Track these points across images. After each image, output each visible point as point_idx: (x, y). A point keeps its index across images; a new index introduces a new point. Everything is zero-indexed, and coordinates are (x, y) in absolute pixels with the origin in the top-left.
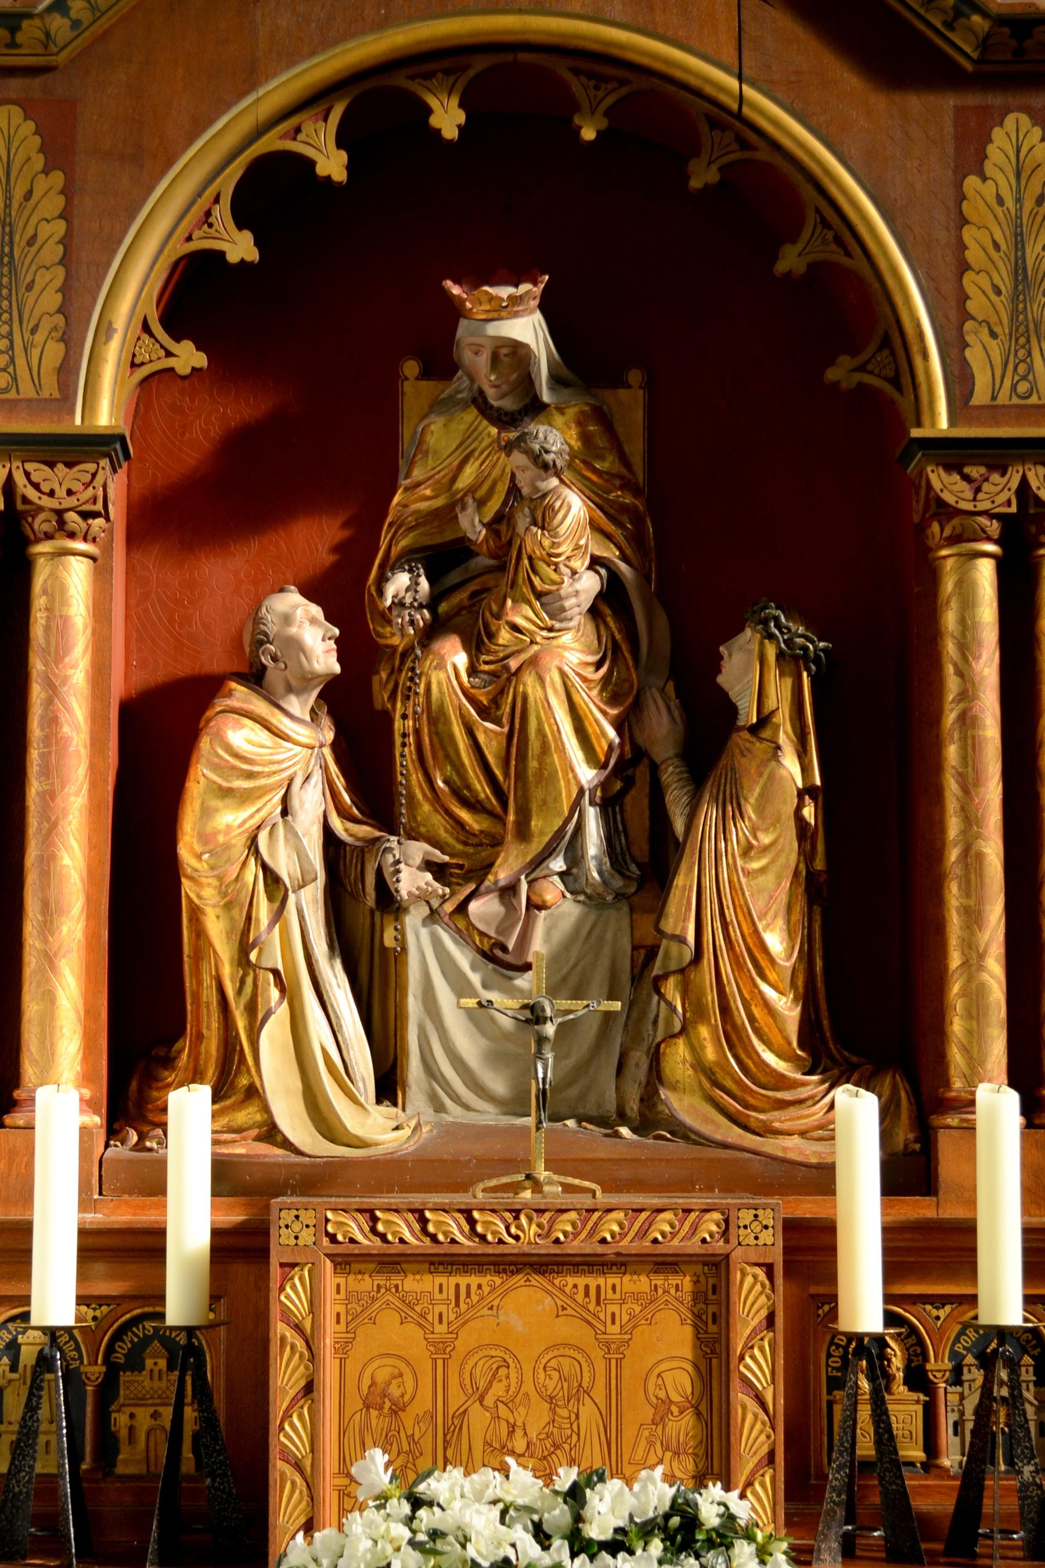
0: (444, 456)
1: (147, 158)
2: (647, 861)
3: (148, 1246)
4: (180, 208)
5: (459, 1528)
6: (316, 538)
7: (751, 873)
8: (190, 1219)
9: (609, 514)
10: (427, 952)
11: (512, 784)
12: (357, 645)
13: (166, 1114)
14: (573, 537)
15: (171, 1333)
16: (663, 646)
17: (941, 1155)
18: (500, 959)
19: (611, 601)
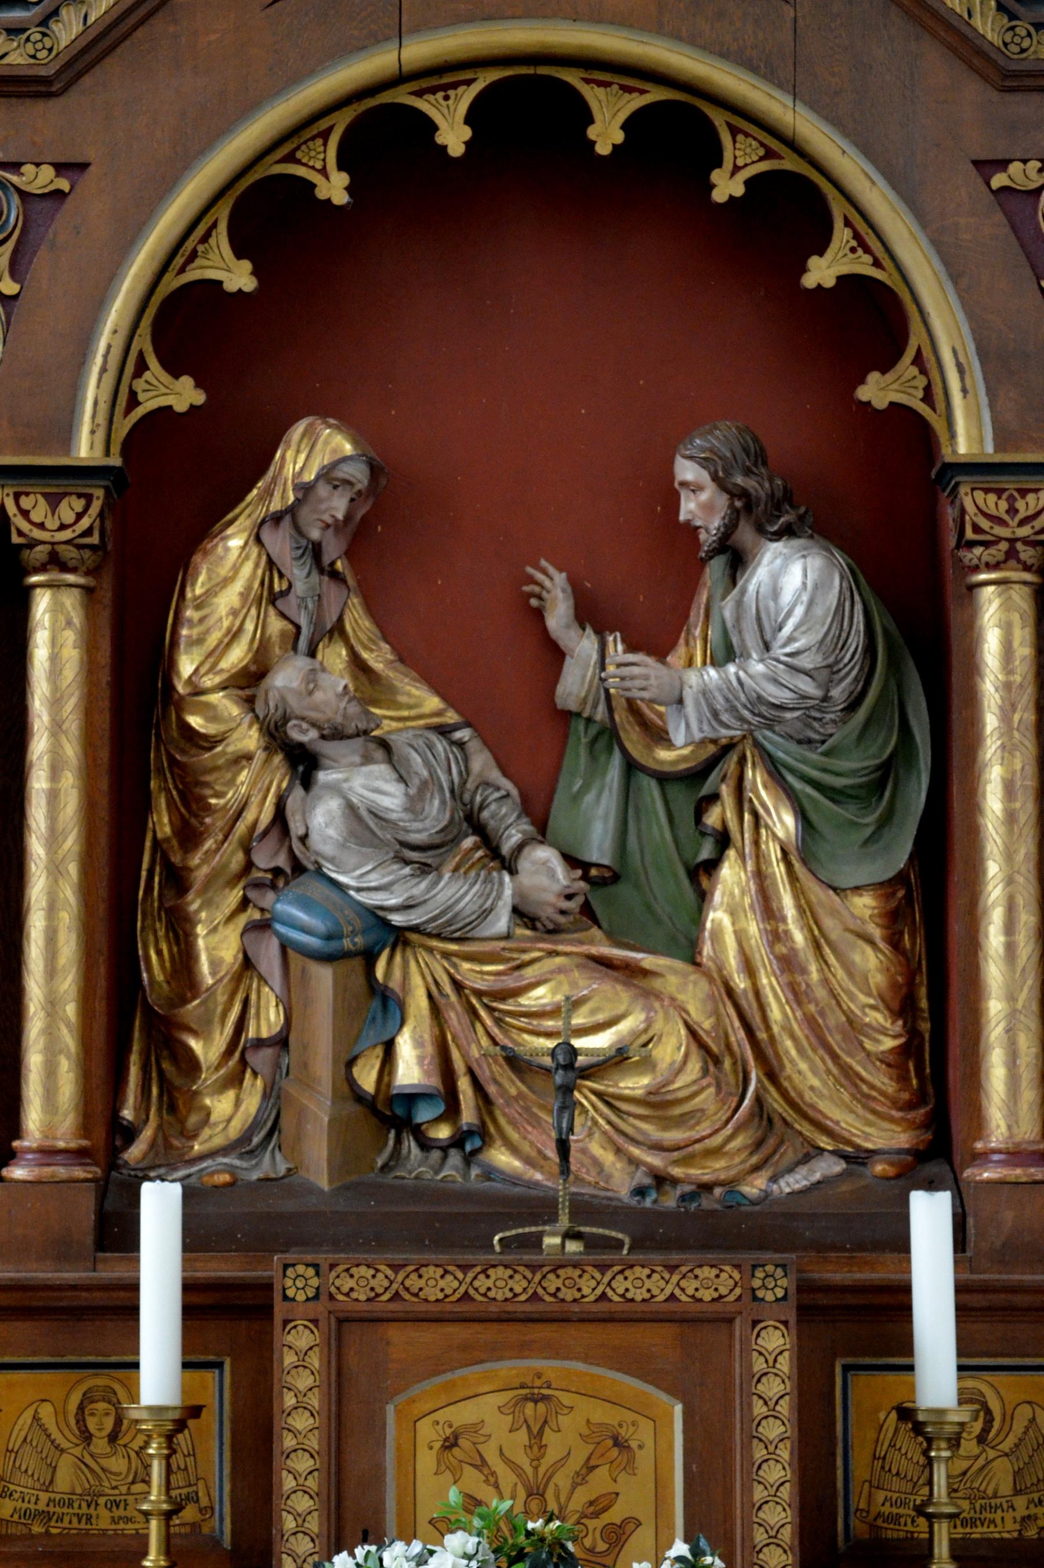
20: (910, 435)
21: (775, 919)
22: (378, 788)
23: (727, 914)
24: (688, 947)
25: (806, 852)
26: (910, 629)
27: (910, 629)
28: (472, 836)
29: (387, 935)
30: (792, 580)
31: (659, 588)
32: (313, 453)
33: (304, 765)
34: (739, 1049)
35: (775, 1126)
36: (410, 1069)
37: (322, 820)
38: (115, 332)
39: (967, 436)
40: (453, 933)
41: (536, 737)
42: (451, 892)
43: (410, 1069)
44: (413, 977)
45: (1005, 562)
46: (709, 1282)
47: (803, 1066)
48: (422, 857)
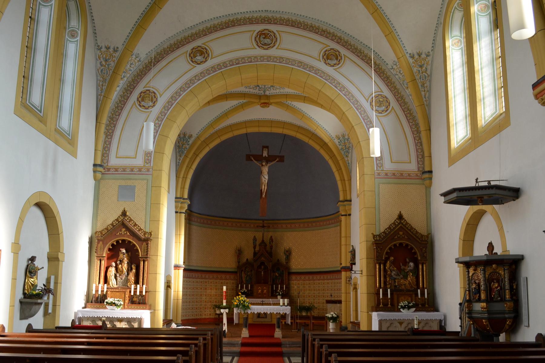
0: (121, 256)
1: (107, 244)
2: (128, 274)
3: (103, 291)
4: (109, 246)
5: (150, 234)
6: (115, 260)
7: (132, 277)
8: (105, 290)
9: (128, 259)
10: (118, 279)
11: (122, 271)
12: (116, 265)
13: (48, 254)
14: (126, 261)
15: (262, 291)
16: (130, 264)
17: (508, 74)
18: (122, 279)
19: (128, 263)
20: (417, 258)
21: (411, 278)
22: (394, 272)
23: (409, 279)
24: (407, 279)
25: (412, 275)
26: (416, 266)
27: (416, 266)
28: (398, 275)
29: (395, 279)
30: (412, 264)
31: (406, 264)
32: (392, 258)
33: (391, 271)
34: (410, 283)
35: (412, 287)
36: (396, 284)
37: (393, 274)
38: (401, 323)
39: (419, 258)
40: (398, 279)
41: (399, 269)
42: (398, 277)
43: (396, 284)
44: (397, 281)
45: (470, 318)
46: (411, 293)
47: (278, 91)
48: (397, 275)
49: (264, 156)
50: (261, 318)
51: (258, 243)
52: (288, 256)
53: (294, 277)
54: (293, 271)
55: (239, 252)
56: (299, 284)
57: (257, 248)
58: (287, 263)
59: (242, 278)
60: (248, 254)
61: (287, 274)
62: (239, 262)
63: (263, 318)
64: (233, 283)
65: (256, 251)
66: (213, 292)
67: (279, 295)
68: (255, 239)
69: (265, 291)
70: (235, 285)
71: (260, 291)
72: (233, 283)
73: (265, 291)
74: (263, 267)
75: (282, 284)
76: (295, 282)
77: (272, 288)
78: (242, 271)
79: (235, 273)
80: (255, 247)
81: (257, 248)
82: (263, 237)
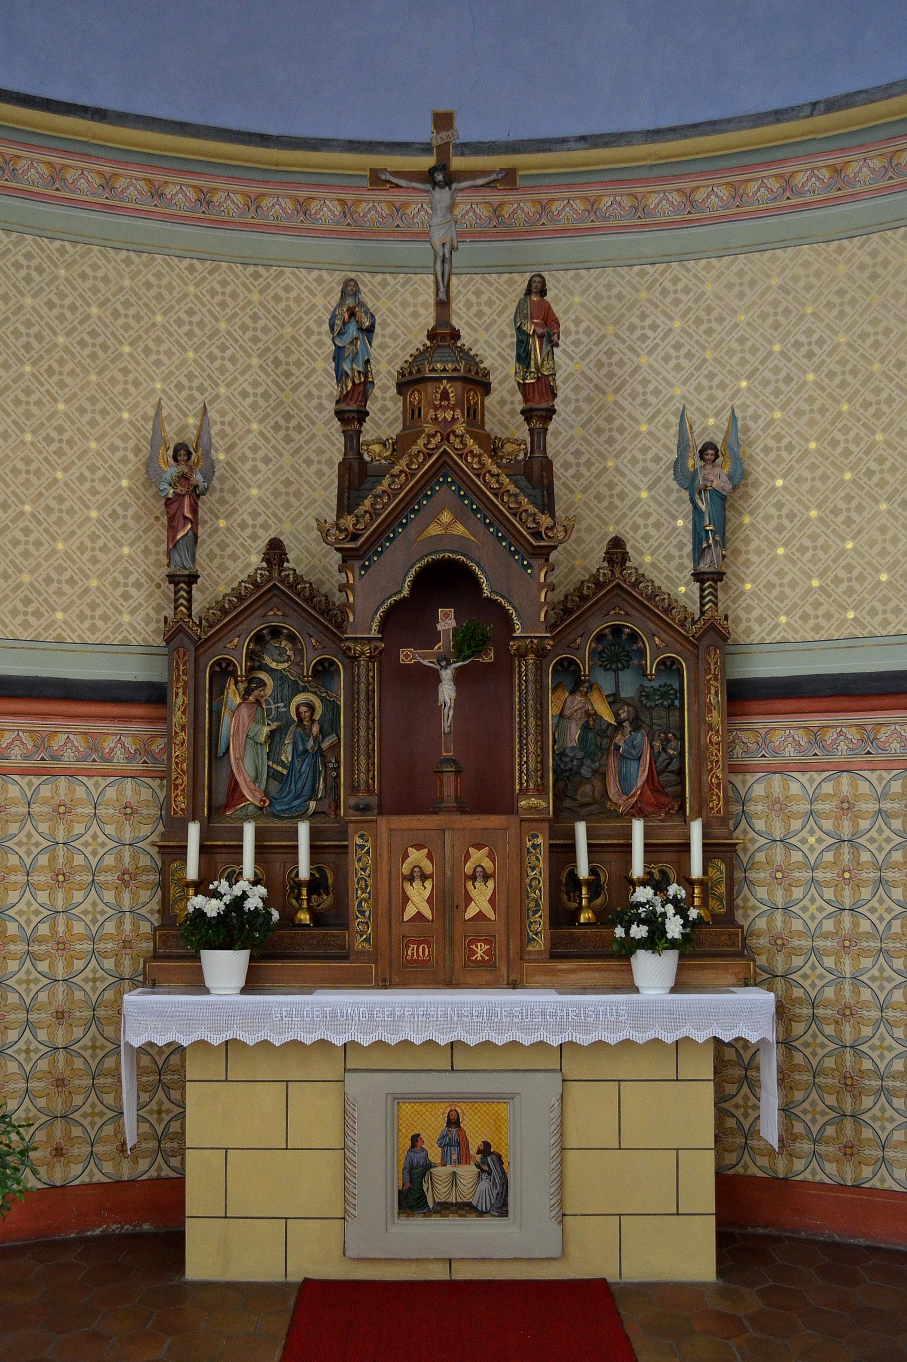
15: (448, 900)
49: (410, 912)
50: (444, 1209)
51: (388, 356)
52: (721, 500)
53: (781, 734)
54: (763, 667)
55: (183, 488)
56: (847, 807)
57: (385, 415)
58: (709, 579)
59: (218, 757)
60: (278, 498)
61: (716, 697)
62: (184, 581)
63: (465, 1208)
64: (129, 811)
65: (375, 453)
66: (36, 878)
67: (656, 940)
68: (353, 322)
69: (481, 897)
70: (148, 831)
71: (419, 897)
72: (129, 811)
73: (481, 897)
74: (446, 622)
75: (666, 796)
76: (797, 785)
77: (563, 851)
78: (223, 671)
79: (153, 696)
80: (351, 413)
81: (385, 415)
82: (443, 305)
